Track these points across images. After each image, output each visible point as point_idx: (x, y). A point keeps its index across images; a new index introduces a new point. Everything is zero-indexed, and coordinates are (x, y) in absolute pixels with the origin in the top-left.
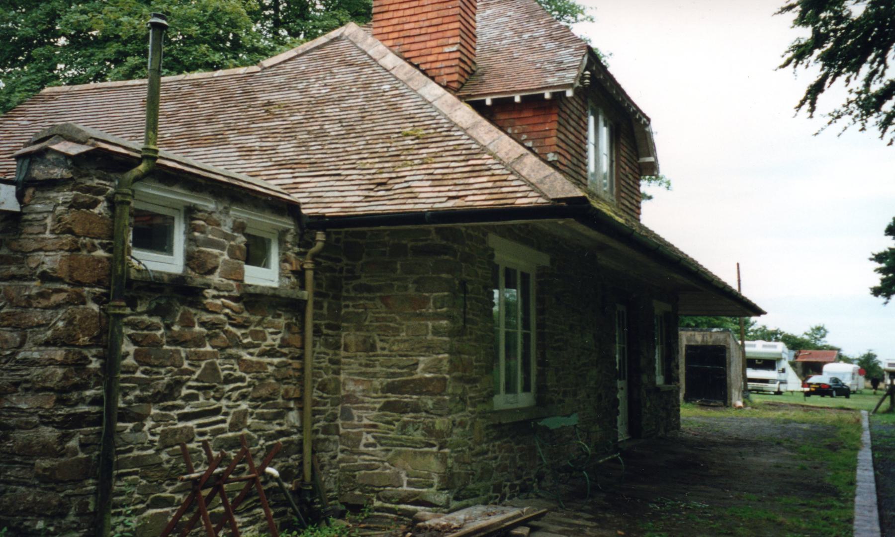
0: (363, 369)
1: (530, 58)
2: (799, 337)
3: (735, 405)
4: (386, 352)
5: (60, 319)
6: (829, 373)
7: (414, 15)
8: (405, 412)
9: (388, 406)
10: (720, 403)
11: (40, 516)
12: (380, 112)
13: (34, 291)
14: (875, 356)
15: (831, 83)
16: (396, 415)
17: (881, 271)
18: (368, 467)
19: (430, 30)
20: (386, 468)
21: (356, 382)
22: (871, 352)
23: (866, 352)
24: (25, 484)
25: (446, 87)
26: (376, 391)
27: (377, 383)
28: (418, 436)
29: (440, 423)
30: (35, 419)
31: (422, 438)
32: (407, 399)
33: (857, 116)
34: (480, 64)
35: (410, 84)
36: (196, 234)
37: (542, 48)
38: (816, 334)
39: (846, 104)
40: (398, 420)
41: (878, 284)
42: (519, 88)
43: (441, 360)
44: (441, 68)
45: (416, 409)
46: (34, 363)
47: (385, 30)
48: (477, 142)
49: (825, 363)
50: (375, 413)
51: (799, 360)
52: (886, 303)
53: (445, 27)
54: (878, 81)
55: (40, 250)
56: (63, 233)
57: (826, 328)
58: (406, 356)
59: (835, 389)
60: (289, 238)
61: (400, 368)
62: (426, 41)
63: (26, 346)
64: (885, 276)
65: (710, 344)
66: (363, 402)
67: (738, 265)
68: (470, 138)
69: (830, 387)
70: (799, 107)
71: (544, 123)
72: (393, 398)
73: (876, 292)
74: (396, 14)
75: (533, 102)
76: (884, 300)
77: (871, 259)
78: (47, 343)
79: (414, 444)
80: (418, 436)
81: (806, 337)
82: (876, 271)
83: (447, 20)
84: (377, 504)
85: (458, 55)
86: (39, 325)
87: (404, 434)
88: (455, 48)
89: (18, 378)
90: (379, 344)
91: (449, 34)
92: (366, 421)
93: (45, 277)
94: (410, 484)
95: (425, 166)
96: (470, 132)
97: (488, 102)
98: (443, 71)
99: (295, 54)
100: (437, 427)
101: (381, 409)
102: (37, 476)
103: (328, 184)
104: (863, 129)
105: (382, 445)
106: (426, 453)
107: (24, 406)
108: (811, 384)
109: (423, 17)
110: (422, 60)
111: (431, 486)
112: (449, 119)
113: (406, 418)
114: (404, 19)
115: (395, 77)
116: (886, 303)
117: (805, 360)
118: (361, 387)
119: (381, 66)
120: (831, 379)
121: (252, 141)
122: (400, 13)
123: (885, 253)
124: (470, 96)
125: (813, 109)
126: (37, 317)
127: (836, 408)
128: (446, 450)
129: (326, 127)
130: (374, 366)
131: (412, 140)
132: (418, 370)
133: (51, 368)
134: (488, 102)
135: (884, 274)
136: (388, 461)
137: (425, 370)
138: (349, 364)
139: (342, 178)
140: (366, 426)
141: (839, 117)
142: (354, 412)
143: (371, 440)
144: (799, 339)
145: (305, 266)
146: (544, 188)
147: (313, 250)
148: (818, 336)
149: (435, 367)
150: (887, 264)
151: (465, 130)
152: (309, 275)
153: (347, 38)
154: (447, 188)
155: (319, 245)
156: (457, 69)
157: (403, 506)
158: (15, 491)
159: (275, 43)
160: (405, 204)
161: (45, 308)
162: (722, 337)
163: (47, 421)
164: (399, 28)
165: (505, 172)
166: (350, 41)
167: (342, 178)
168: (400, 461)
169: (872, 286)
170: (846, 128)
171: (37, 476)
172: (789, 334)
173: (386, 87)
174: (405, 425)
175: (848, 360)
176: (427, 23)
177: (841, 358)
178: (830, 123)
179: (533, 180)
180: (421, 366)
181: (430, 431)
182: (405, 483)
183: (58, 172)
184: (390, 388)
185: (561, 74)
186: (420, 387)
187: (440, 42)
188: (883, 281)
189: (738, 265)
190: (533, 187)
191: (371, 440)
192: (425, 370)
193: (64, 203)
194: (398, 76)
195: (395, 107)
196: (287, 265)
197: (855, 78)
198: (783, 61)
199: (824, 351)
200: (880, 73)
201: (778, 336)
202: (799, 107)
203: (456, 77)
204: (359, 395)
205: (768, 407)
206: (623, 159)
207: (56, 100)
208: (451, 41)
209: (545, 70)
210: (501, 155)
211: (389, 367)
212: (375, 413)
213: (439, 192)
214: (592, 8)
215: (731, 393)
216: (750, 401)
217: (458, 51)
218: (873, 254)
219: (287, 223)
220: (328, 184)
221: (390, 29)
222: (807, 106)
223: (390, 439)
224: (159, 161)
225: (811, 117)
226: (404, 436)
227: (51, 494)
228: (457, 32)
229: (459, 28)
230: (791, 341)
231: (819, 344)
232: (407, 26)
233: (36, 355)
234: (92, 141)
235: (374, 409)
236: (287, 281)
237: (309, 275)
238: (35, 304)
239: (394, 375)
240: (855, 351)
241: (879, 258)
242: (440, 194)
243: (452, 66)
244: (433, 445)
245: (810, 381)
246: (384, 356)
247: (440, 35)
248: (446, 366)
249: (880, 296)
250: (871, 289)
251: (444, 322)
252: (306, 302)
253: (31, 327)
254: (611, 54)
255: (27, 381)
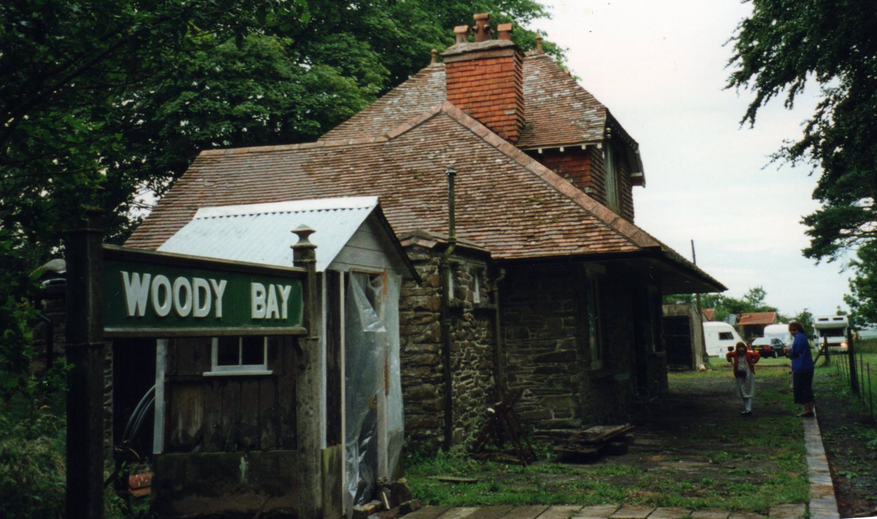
0: (520, 349)
1: (564, 116)
2: (739, 301)
3: (699, 368)
4: (535, 338)
5: (428, 330)
6: (770, 335)
7: (479, 86)
8: (550, 374)
9: (538, 371)
10: (686, 367)
11: (427, 428)
12: (505, 182)
13: (412, 316)
14: (811, 315)
15: (766, 101)
16: (544, 376)
17: (811, 233)
18: (529, 409)
19: (493, 98)
20: (539, 408)
21: (516, 358)
22: (807, 311)
23: (802, 311)
24: (417, 413)
25: (509, 140)
26: (530, 362)
27: (530, 357)
28: (559, 387)
29: (572, 378)
30: (420, 380)
31: (561, 388)
32: (551, 365)
33: (789, 157)
34: (528, 119)
35: (517, 160)
36: (459, 278)
37: (570, 108)
38: (755, 296)
39: (781, 149)
40: (546, 379)
41: (809, 245)
42: (562, 141)
43: (571, 341)
44: (503, 126)
45: (557, 371)
46: (416, 352)
47: (457, 96)
48: (582, 208)
49: (765, 325)
50: (531, 376)
51: (741, 323)
52: (817, 264)
53: (504, 96)
54: (800, 92)
55: (414, 295)
56: (427, 286)
57: (764, 289)
58: (548, 339)
59: (777, 350)
60: (484, 273)
61: (544, 346)
62: (490, 106)
63: (409, 345)
64: (814, 238)
65: (676, 315)
66: (522, 369)
67: (692, 242)
68: (577, 204)
69: (772, 348)
70: (742, 122)
71: (581, 166)
72: (541, 366)
73: (808, 253)
74: (465, 85)
75: (573, 151)
76: (815, 260)
77: (801, 223)
78: (422, 342)
79: (558, 392)
80: (559, 387)
81: (746, 300)
82: (805, 233)
83: (506, 90)
84: (536, 430)
85: (515, 117)
86: (416, 333)
87: (551, 386)
88: (513, 112)
89: (407, 361)
90: (530, 334)
91: (508, 101)
92: (525, 381)
93: (419, 309)
94: (556, 416)
95: (555, 224)
96: (576, 200)
97: (540, 151)
98: (505, 129)
99: (410, 127)
100: (572, 381)
101: (534, 373)
102: (424, 409)
103: (494, 237)
104: (793, 166)
105: (536, 395)
106: (565, 397)
107: (413, 375)
108: (755, 346)
109: (486, 88)
110: (488, 120)
111: (569, 416)
112: (556, 189)
113: (551, 377)
114: (471, 89)
115: (501, 152)
116: (817, 264)
117: (746, 323)
118: (520, 361)
119: (486, 142)
120: (772, 340)
121: (419, 203)
122: (468, 84)
123: (814, 216)
124: (526, 147)
125: (753, 121)
126: (415, 329)
127: (781, 366)
128: (578, 394)
129: (469, 192)
130: (528, 347)
131: (538, 205)
132: (557, 347)
133: (426, 355)
134: (540, 151)
135: (813, 236)
136: (541, 404)
137: (561, 347)
138: (511, 347)
139: (502, 232)
140: (525, 384)
141: (777, 158)
142: (517, 376)
143: (529, 392)
144: (739, 303)
145: (494, 289)
146: (636, 240)
147: (498, 279)
148: (757, 298)
149: (567, 345)
150: (816, 226)
151: (572, 199)
152: (496, 294)
153: (446, 113)
154: (575, 240)
155: (503, 276)
156: (516, 127)
157: (553, 430)
158: (411, 417)
159: (754, 306)
160: (552, 250)
161: (418, 325)
162: (684, 308)
163: (426, 381)
164: (468, 95)
165: (607, 229)
166: (449, 116)
167: (502, 232)
168: (549, 403)
169: (804, 249)
170: (782, 165)
171: (424, 409)
172: (730, 298)
173: (499, 161)
174: (551, 381)
175: (785, 321)
176: (490, 92)
177: (780, 319)
178: (771, 162)
179: (628, 236)
180: (558, 345)
181: (567, 383)
182: (553, 417)
183: (422, 256)
184: (537, 361)
185: (591, 131)
186: (560, 357)
187: (501, 106)
188: (813, 242)
189: (692, 242)
190: (629, 240)
191: (529, 392)
192: (561, 347)
193: (427, 271)
194: (506, 153)
195: (512, 178)
196: (484, 290)
197: (782, 90)
198: (728, 83)
199: (763, 313)
200: (801, 85)
201: (720, 300)
202: (742, 122)
203: (515, 133)
204: (519, 365)
205: (725, 369)
206: (622, 177)
207: (219, 162)
208: (509, 106)
209: (579, 128)
210: (602, 217)
211: (538, 347)
212: (531, 376)
213: (571, 242)
214: (549, 7)
215: (695, 359)
216: (710, 365)
217: (516, 114)
218: (803, 218)
219: (483, 264)
220: (494, 237)
221: (461, 96)
222: (749, 119)
223: (542, 390)
224: (457, 244)
225: (752, 127)
226: (551, 388)
227: (432, 417)
228: (514, 100)
229: (515, 97)
230: (732, 305)
231: (759, 306)
232: (474, 94)
233: (416, 349)
234: (434, 239)
235: (530, 373)
236: (485, 299)
237: (496, 294)
238: (412, 323)
239: (541, 352)
240: (792, 312)
241: (809, 221)
242: (572, 244)
243: (511, 125)
244: (569, 392)
245: (754, 343)
246: (533, 340)
247: (501, 101)
248: (574, 343)
249: (811, 257)
250: (803, 251)
251: (571, 318)
252: (495, 311)
253: (411, 334)
254: (568, 49)
255: (413, 362)
